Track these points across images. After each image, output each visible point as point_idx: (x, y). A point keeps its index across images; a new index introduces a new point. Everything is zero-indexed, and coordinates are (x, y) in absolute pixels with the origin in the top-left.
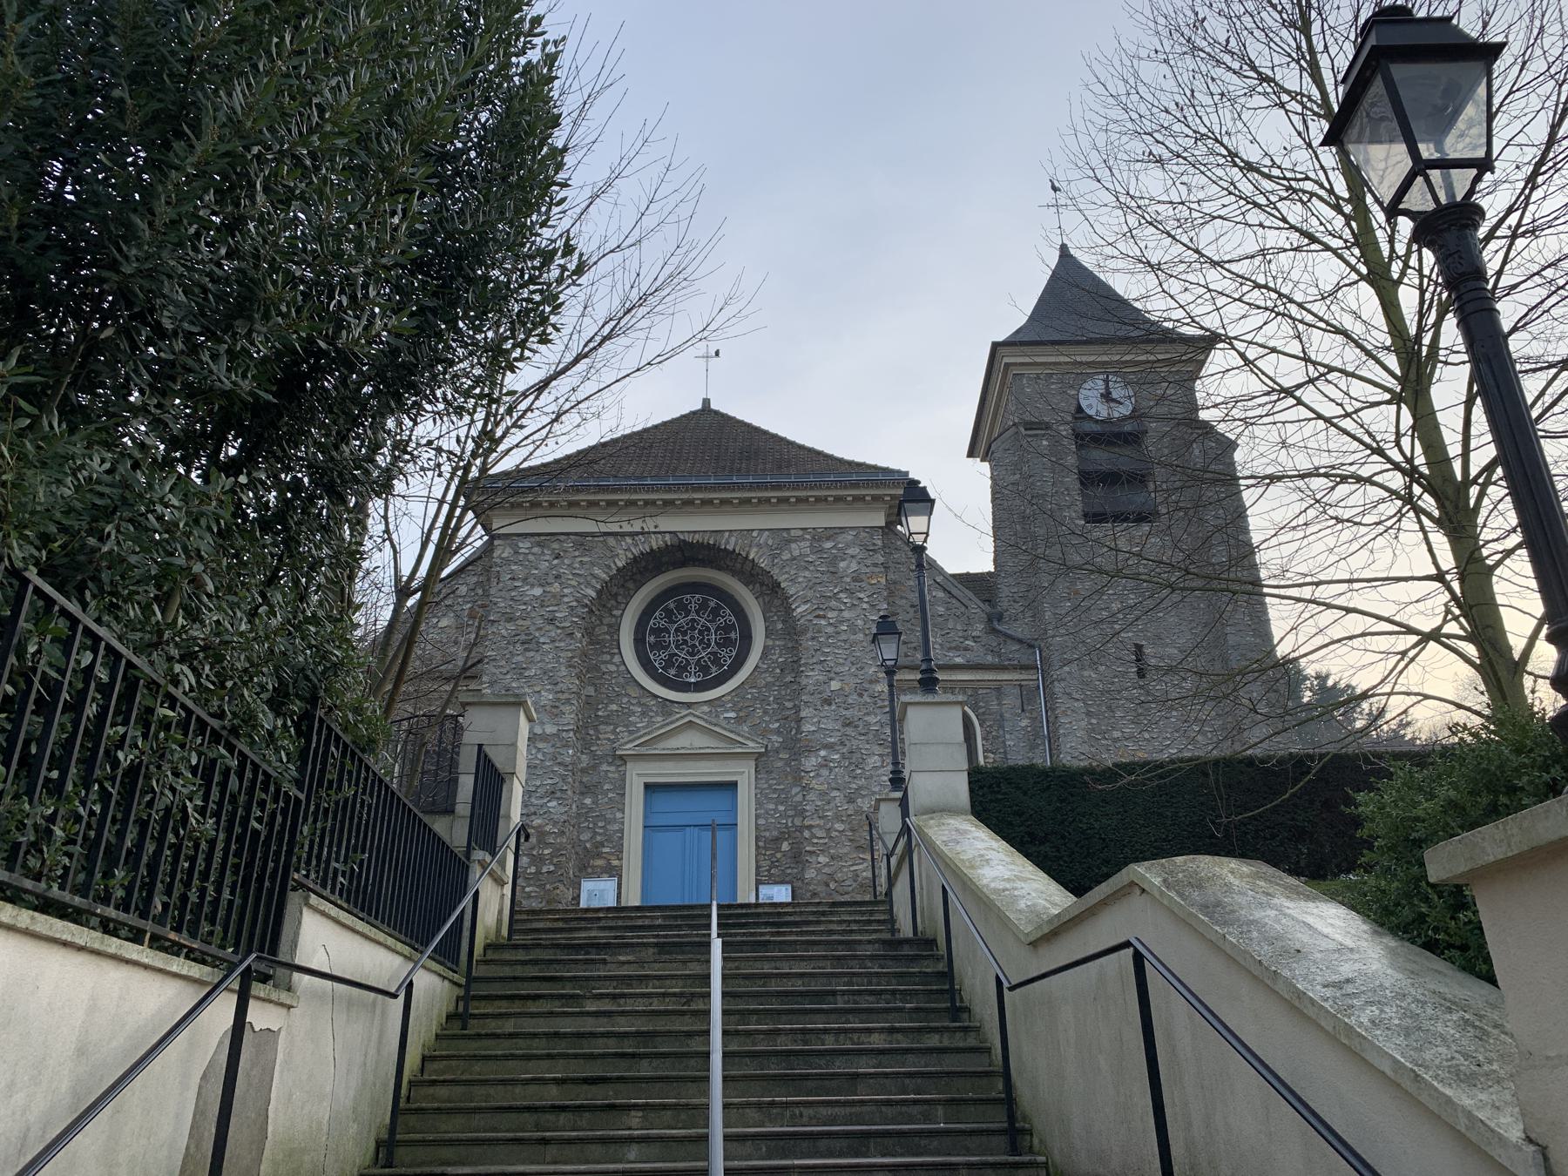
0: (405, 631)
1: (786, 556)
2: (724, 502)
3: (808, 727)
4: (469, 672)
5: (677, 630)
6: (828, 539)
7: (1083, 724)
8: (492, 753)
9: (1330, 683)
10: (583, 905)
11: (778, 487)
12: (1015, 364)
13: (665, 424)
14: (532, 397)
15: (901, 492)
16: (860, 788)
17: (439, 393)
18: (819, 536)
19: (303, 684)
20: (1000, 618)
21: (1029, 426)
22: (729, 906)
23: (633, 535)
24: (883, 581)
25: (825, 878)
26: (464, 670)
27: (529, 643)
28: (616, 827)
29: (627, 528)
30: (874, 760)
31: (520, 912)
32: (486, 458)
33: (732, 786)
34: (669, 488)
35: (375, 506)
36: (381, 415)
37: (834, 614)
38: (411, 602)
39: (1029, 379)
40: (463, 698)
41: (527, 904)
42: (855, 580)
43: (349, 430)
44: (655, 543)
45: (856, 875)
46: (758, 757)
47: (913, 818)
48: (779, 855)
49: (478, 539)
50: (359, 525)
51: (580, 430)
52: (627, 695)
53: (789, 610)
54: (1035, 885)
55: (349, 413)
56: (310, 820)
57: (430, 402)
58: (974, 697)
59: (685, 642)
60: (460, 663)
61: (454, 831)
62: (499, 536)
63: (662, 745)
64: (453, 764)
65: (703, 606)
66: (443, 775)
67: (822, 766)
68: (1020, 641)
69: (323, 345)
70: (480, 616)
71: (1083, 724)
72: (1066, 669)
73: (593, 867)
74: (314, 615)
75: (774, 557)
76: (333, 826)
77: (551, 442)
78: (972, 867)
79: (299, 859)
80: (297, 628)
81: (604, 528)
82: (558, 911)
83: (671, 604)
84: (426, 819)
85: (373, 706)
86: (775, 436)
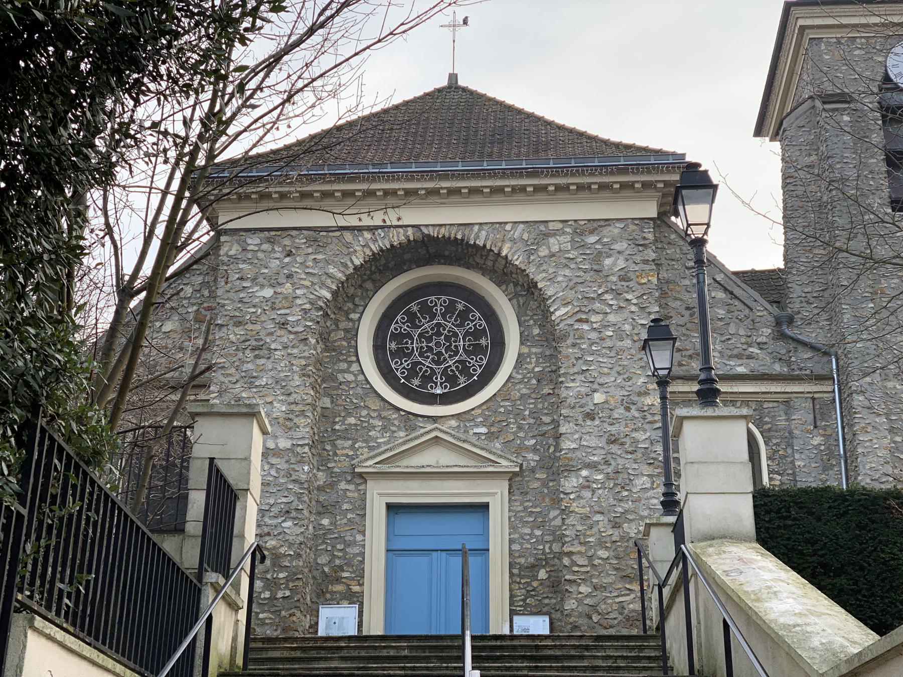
0: (130, 333)
1: (544, 251)
2: (473, 191)
3: (567, 444)
4: (197, 381)
5: (420, 336)
6: (592, 232)
7: (886, 441)
8: (226, 469)
10: (321, 633)
11: (534, 173)
12: (812, 27)
13: (406, 103)
14: (262, 74)
15: (676, 177)
16: (626, 512)
17: (163, 69)
18: (581, 229)
19: (23, 390)
20: (791, 320)
21: (827, 99)
22: (483, 638)
23: (372, 229)
24: (654, 280)
25: (586, 609)
26: (193, 377)
27: (260, 349)
28: (356, 550)
29: (367, 221)
30: (642, 482)
31: (255, 640)
32: (215, 141)
33: (484, 508)
34: (410, 176)
35: (94, 195)
36: (99, 93)
37: (599, 317)
38: (133, 304)
39: (829, 44)
40: (192, 408)
41: (259, 632)
42: (622, 279)
43: (66, 112)
44: (397, 238)
45: (622, 607)
46: (512, 477)
47: (690, 545)
48: (535, 584)
49: (204, 233)
50: (79, 217)
51: (317, 110)
52: (366, 407)
53: (546, 313)
54: (830, 621)
55: (62, 93)
56: (33, 537)
57: (154, 80)
58: (759, 414)
59: (430, 349)
60: (188, 370)
61: (185, 552)
62: (226, 232)
63: (405, 462)
64: (183, 480)
65: (450, 309)
66: (171, 491)
67: (584, 487)
68: (813, 348)
69: (39, 15)
70: (207, 321)
71: (886, 441)
72: (868, 379)
73: (332, 593)
74: (33, 316)
75: (530, 253)
76: (58, 543)
77: (282, 125)
78: (758, 600)
79: (23, 578)
80: (16, 330)
81: (342, 222)
82: (296, 639)
84: (155, 538)
85: (98, 416)
86: (530, 116)
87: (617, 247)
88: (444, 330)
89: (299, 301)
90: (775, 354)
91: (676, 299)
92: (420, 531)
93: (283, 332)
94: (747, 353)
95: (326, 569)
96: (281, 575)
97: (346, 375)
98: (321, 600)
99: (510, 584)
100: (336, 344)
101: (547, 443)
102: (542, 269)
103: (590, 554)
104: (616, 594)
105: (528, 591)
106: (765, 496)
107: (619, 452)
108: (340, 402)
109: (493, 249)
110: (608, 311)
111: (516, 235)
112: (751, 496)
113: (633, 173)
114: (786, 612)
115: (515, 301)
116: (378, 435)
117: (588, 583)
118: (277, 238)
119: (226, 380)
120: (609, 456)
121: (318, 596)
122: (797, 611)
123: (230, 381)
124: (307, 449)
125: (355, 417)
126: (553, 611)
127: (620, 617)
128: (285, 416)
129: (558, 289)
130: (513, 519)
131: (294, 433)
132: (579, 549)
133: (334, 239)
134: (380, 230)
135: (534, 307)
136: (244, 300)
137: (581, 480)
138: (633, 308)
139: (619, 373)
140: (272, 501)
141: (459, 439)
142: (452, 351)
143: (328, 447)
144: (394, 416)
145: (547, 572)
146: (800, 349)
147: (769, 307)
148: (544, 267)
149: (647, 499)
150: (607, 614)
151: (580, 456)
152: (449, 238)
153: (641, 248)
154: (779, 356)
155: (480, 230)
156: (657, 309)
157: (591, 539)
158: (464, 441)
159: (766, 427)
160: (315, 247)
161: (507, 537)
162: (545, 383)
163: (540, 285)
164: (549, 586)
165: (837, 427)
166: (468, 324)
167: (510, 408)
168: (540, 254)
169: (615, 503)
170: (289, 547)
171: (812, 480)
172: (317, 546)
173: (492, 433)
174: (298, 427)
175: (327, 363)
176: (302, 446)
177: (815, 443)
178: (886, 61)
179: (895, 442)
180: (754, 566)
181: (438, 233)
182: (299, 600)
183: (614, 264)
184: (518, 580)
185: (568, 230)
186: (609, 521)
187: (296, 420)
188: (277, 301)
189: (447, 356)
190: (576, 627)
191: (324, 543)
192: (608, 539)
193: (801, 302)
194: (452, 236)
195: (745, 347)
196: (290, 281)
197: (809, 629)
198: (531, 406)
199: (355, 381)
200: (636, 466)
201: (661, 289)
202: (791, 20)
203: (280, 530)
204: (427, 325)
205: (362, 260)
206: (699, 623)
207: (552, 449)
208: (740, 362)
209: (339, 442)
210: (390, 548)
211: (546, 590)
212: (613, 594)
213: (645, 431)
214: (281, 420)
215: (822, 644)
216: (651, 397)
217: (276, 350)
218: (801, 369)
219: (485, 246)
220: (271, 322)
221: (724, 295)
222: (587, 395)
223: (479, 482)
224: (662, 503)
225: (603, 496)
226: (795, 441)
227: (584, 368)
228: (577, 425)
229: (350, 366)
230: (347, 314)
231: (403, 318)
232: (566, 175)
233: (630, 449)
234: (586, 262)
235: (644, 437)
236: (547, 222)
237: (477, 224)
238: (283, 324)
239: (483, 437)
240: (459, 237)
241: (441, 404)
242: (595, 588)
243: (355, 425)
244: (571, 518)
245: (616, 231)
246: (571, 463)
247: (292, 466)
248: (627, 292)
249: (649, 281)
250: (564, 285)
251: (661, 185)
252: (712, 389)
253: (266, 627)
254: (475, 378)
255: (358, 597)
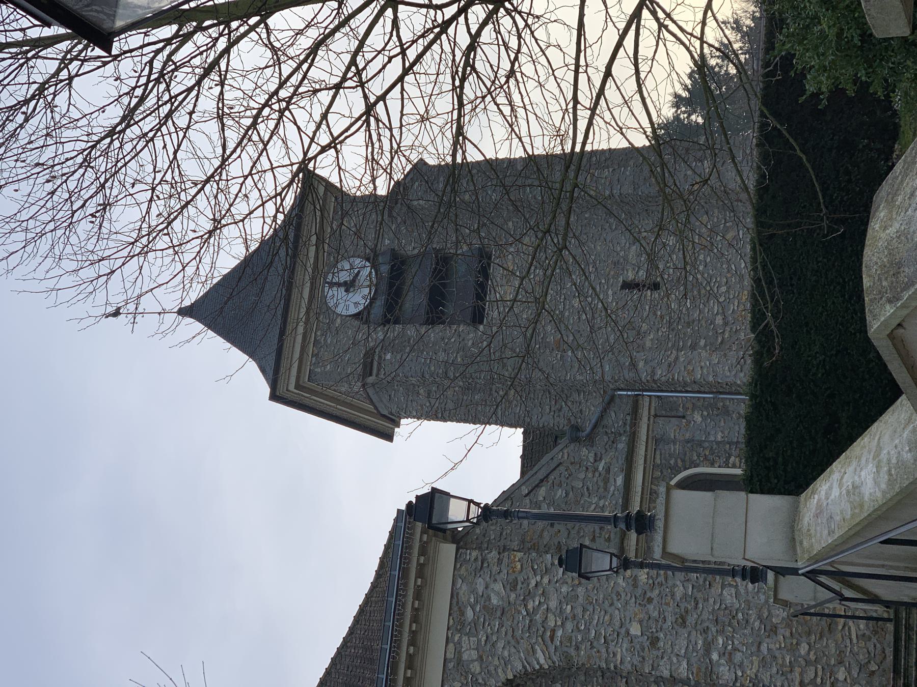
1: (476, 667)
3: (683, 670)
6: (462, 613)
9: (685, 94)
15: (419, 525)
16: (760, 617)
18: (458, 624)
21: (367, 369)
24: (519, 555)
30: (728, 595)
37: (551, 617)
42: (514, 587)
54: (886, 438)
68: (605, 410)
72: (641, 364)
78: (861, 506)
87: (481, 589)
90: (607, 446)
91: (541, 536)
94: (603, 473)
102: (493, 672)
103: (803, 663)
104: (848, 641)
106: (752, 479)
110: (545, 606)
112: (750, 495)
113: (408, 563)
114: (874, 479)
117: (836, 669)
120: (699, 627)
122: (875, 470)
127: (874, 640)
132: (797, 675)
137: (723, 661)
139: (612, 605)
146: (605, 422)
147: (560, 447)
148: (492, 668)
154: (610, 443)
156: (549, 556)
159: (680, 463)
163: (510, 677)
165: (686, 397)
168: (477, 672)
171: (737, 427)
177: (700, 419)
178: (342, 316)
179: (705, 346)
180: (825, 504)
183: (498, 594)
185: (456, 638)
193: (559, 416)
195: (597, 474)
197: (894, 461)
200: (711, 601)
201: (529, 549)
202: (288, 396)
206: (883, 566)
208: (612, 480)
212: (849, 644)
213: (675, 586)
215: (910, 450)
218: (625, 424)
221: (544, 488)
222: (632, 642)
224: (753, 583)
226: (697, 438)
228: (662, 658)
232: (400, 632)
234: (492, 623)
235: (681, 588)
236: (445, 660)
242: (841, 663)
245: (464, 587)
246: (703, 670)
248: (528, 585)
249: (519, 561)
250: (513, 650)
251: (425, 537)
252: (636, 519)
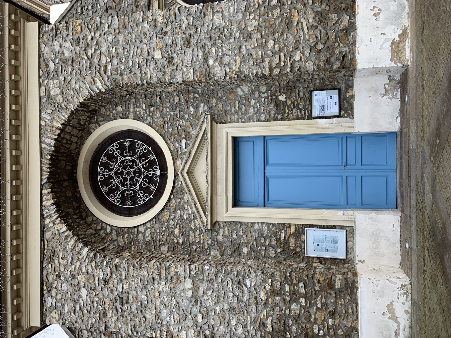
1: (60, 99)
3: (190, 76)
5: (123, 185)
6: (47, 66)
16: (239, 29)
25: (313, 54)
28: (265, 229)
37: (103, 58)
42: (78, 43)
44: (49, 202)
46: (215, 121)
48: (289, 103)
52: (168, 221)
59: (132, 179)
63: (204, 195)
65: (106, 166)
73: (296, 247)
75: (60, 108)
83: (104, 189)
87: (57, 48)
88: (119, 170)
89: (90, 270)
92: (251, 185)
93: (111, 283)
95: (279, 250)
96: (287, 289)
97: (147, 235)
98: (301, 254)
99: (289, 120)
100: (127, 242)
101: (193, 99)
102: (71, 99)
103: (271, 54)
104: (301, 32)
105: (294, 107)
107: (196, 37)
108: (164, 239)
109: (57, 133)
110: (99, 52)
111: (49, 118)
115: (100, 123)
116: (186, 213)
117: (293, 54)
118: (48, 285)
119: (144, 325)
120: (199, 45)
121: (298, 257)
123: (144, 322)
124: (193, 267)
125: (175, 229)
126: (308, 89)
127: (320, 27)
128: (169, 283)
129: (84, 88)
130: (243, 120)
131: (182, 276)
133: (50, 245)
134: (44, 213)
135: (104, 110)
136: (89, 309)
137: (216, 64)
138: (97, 34)
139: (141, 42)
140: (231, 294)
141: (189, 157)
142: (133, 164)
143: (194, 247)
144: (174, 202)
145: (280, 95)
148: (69, 97)
149: (230, 14)
150: (317, 37)
151: (199, 66)
152: (50, 164)
153: (58, 32)
155: (45, 143)
157: (260, 54)
158: (190, 153)
160: (54, 258)
161: (256, 123)
162: (153, 102)
163: (81, 100)
164: (291, 93)
166: (116, 154)
167: (169, 124)
168: (61, 101)
169: (233, 38)
170: (266, 282)
172: (262, 257)
173: (186, 136)
174: (177, 273)
175: (138, 248)
176: (190, 270)
181: (47, 172)
182: (307, 276)
184: (286, 115)
186: (246, 41)
187: (172, 274)
188: (90, 286)
189: (136, 168)
190: (327, 61)
191: (260, 252)
192: (260, 41)
194: (48, 162)
196: (76, 276)
198: (168, 110)
199: (151, 229)
200: (206, 25)
203: (253, 289)
204: (116, 181)
205: (64, 225)
207: (196, 95)
209: (191, 240)
210: (263, 205)
211: (293, 95)
212: (302, 34)
214: (172, 286)
216: (158, 17)
217: (123, 288)
219: (56, 140)
220: (104, 291)
222: (156, 63)
223: (218, 143)
225: (227, 47)
227: (137, 66)
228: (177, 70)
229: (141, 232)
230: (107, 234)
231: (112, 196)
233: (194, 30)
234: (67, 69)
235: (186, 21)
237: (40, 145)
238: (105, 282)
239: (188, 142)
240: (49, 157)
241: (166, 171)
243: (179, 229)
244: (244, 70)
245: (47, 49)
246: (204, 73)
247: (205, 278)
248: (87, 40)
249: (79, 25)
250: (81, 83)
253: (328, 302)
254: (150, 148)
255: (299, 228)
